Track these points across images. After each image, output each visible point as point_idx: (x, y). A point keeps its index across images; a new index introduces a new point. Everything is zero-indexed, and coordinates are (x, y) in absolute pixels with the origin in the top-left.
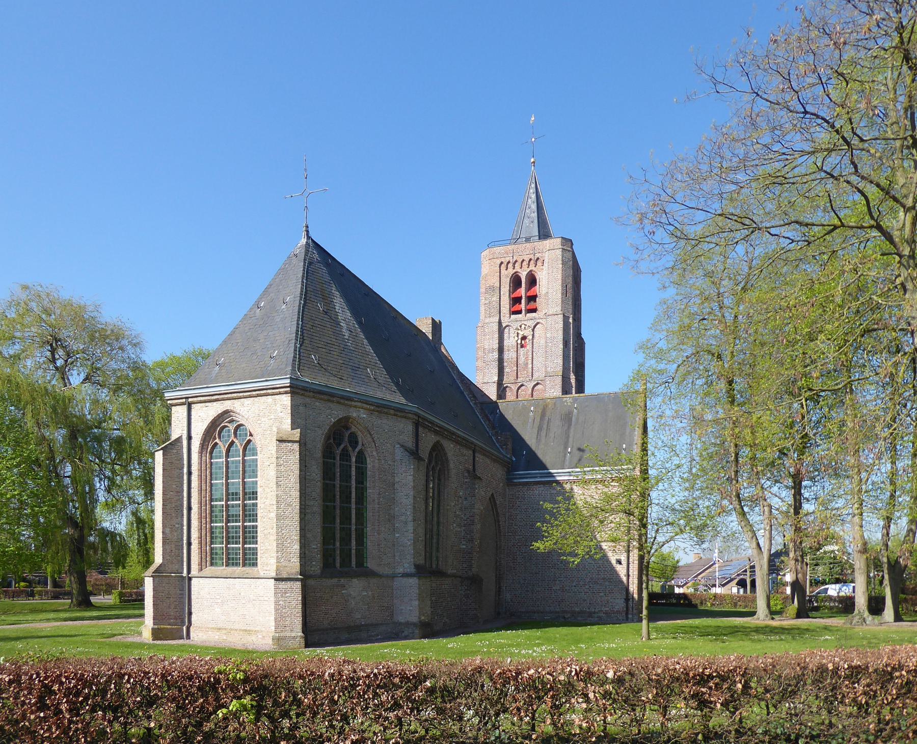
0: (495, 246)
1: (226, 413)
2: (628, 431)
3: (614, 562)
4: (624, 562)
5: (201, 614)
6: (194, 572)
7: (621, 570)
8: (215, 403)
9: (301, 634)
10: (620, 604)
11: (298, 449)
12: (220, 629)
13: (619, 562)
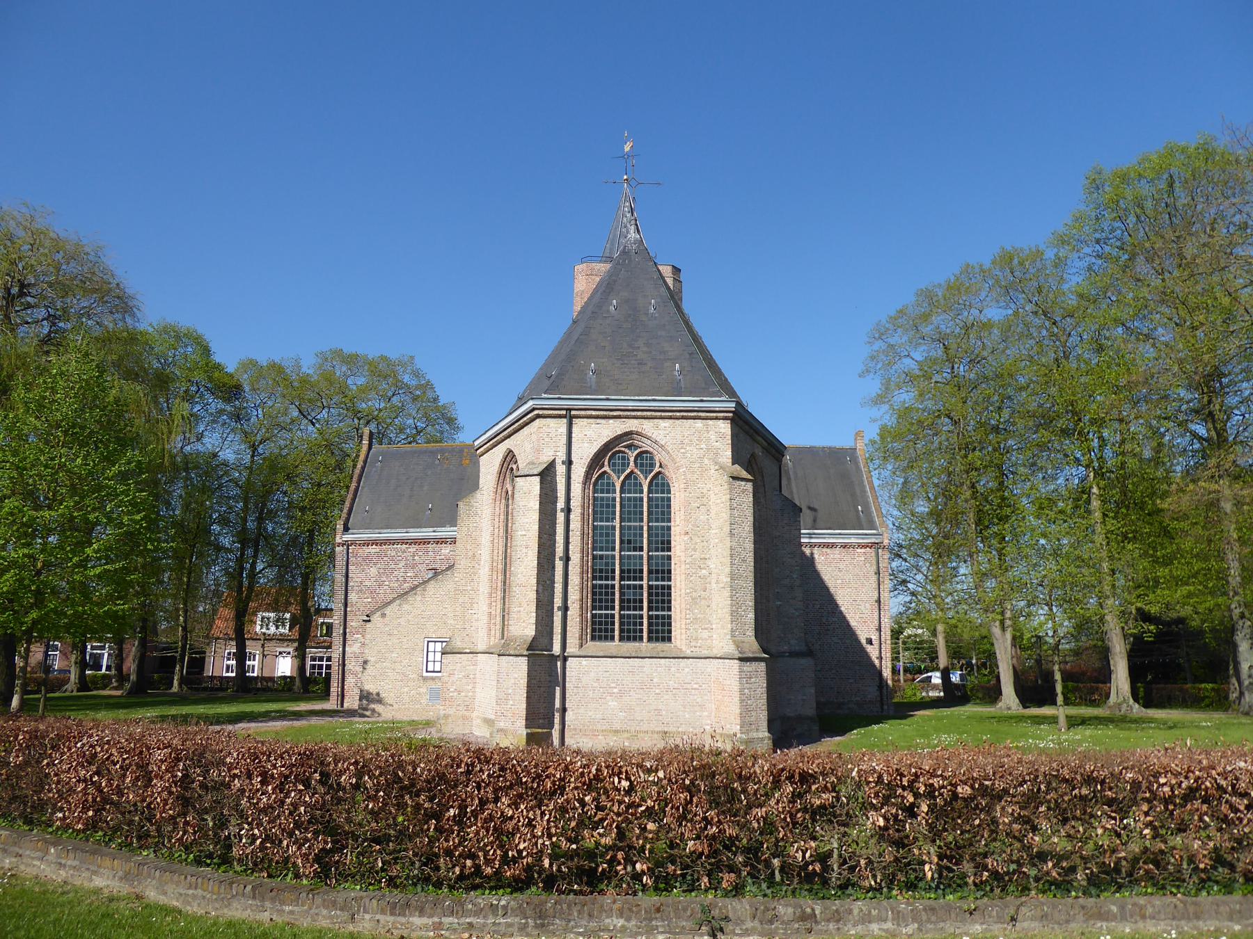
0: (592, 262)
1: (628, 435)
2: (858, 492)
3: (864, 641)
4: (875, 642)
5: (582, 711)
6: (570, 650)
7: (873, 652)
8: (611, 421)
9: (767, 734)
10: (872, 692)
11: (751, 490)
12: (617, 731)
13: (870, 642)
